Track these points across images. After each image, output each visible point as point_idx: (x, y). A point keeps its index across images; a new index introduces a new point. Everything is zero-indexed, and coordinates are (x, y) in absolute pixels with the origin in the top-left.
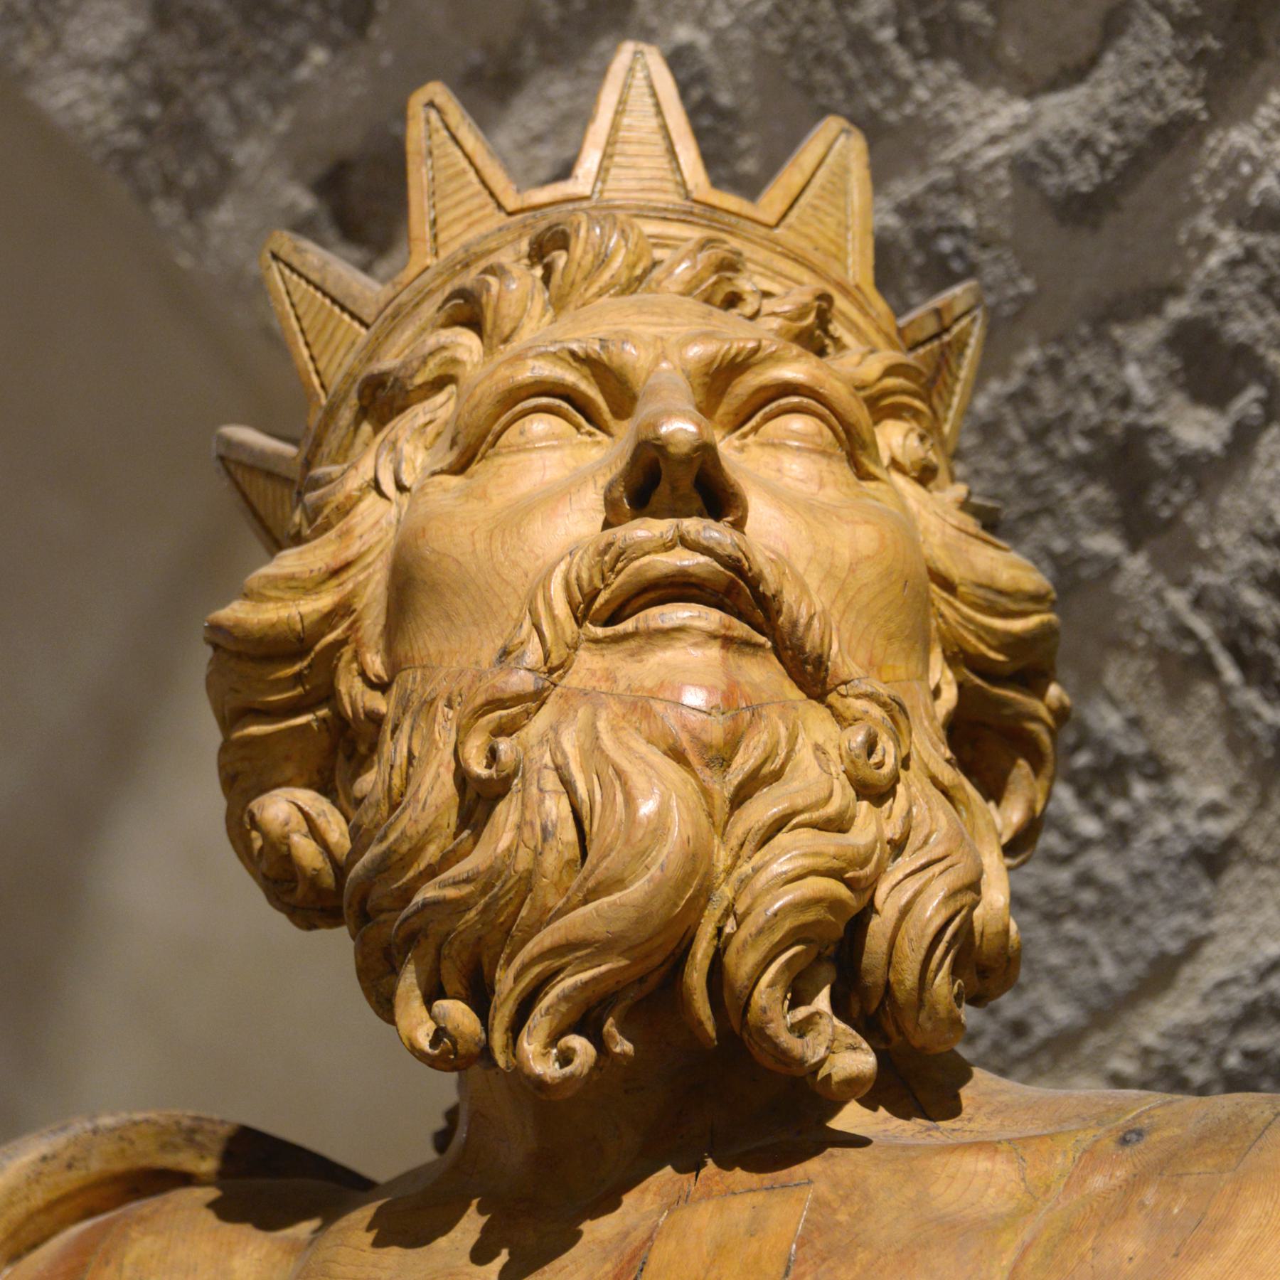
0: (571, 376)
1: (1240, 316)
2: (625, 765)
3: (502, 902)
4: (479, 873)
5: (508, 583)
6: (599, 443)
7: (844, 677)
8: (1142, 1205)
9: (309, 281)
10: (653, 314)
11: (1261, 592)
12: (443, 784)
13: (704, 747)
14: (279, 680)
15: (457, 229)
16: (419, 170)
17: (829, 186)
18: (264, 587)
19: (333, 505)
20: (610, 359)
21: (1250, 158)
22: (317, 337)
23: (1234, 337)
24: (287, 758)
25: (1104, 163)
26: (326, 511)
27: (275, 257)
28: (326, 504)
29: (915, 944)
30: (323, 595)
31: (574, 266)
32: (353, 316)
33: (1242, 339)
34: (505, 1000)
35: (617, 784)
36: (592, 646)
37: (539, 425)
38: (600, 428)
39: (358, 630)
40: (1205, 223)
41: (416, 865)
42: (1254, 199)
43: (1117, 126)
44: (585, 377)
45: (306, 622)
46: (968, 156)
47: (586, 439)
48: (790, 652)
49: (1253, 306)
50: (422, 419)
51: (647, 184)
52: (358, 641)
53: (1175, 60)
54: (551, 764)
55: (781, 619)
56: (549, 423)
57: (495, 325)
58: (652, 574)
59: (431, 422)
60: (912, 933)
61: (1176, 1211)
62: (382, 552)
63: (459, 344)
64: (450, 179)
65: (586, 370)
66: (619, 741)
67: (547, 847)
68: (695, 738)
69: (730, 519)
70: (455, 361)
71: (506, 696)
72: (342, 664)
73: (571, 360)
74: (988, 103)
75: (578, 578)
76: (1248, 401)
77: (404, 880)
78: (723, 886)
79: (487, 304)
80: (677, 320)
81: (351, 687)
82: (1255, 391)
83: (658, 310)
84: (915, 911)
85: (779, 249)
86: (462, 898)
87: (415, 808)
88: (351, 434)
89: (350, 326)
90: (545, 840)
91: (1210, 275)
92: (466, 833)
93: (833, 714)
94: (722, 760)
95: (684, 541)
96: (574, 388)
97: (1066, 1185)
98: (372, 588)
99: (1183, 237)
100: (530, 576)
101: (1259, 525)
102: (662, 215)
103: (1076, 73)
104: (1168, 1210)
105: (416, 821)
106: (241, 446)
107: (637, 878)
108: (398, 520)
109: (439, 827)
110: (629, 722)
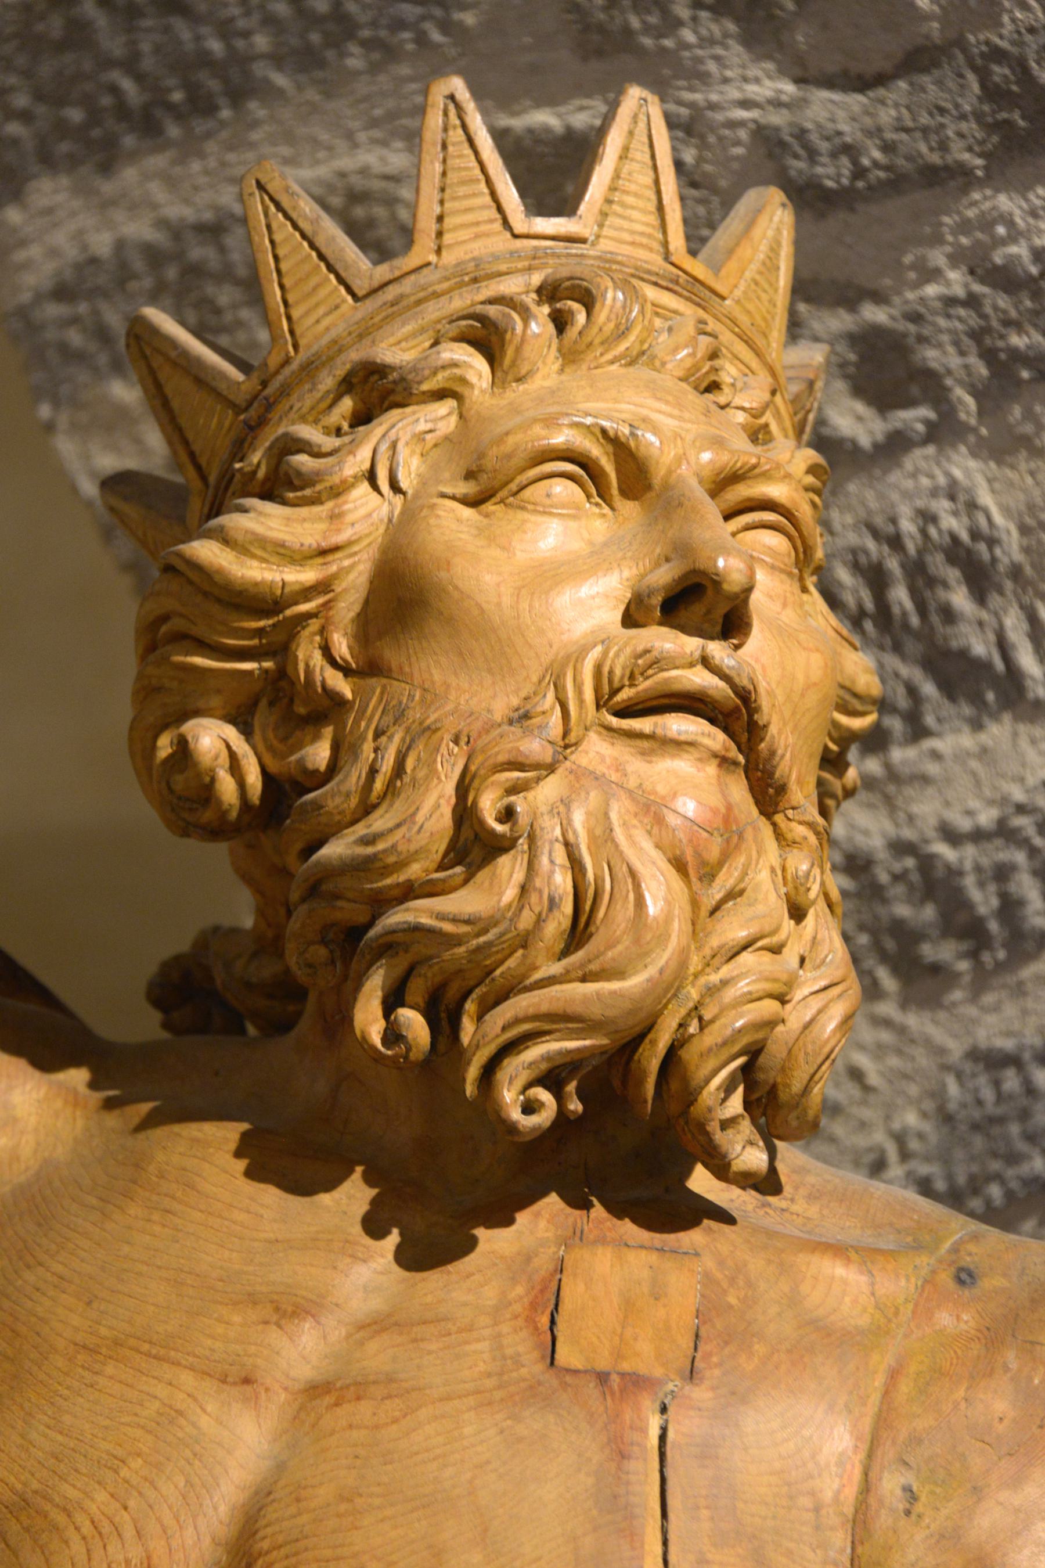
0: (596, 451)
1: (940, 346)
2: (638, 866)
3: (494, 949)
4: (480, 919)
5: (530, 646)
6: (604, 515)
7: (794, 803)
8: (1006, 1369)
9: (295, 226)
10: (667, 402)
11: (854, 575)
12: (442, 815)
13: (704, 863)
14: (243, 629)
15: (463, 235)
16: (432, 162)
17: (768, 262)
18: (251, 543)
19: (328, 484)
20: (637, 447)
21: (1010, 223)
22: (296, 284)
23: (924, 359)
24: (219, 691)
25: (859, 172)
26: (319, 487)
27: (260, 186)
28: (320, 481)
29: (810, 1059)
30: (307, 568)
31: (595, 330)
32: (341, 280)
33: (933, 365)
34: (489, 1042)
35: (629, 881)
36: (604, 732)
37: (561, 488)
38: (605, 501)
39: (330, 608)
40: (938, 258)
41: (395, 876)
42: (998, 258)
43: (888, 148)
44: (607, 454)
45: (287, 590)
46: (713, 107)
47: (596, 510)
48: (759, 774)
49: (956, 343)
50: (422, 426)
51: (638, 239)
52: (327, 619)
53: (971, 118)
54: (561, 838)
55: (763, 745)
56: (566, 487)
57: (514, 363)
58: (677, 687)
59: (430, 431)
60: (810, 1048)
61: (1036, 1381)
62: (369, 544)
63: (471, 367)
64: (463, 183)
65: (610, 448)
66: (630, 837)
67: (551, 917)
68: (698, 854)
69: (735, 641)
70: (463, 381)
71: (528, 762)
72: (306, 633)
73: (600, 436)
74: (753, 72)
75: (611, 672)
76: (915, 417)
77: (380, 884)
78: (689, 987)
79: (511, 341)
80: (687, 415)
81: (310, 657)
82: (925, 412)
83: (670, 398)
84: (815, 1028)
85: (737, 330)
86: (458, 935)
87: (409, 829)
88: (329, 401)
89: (336, 289)
90: (550, 909)
91: (922, 300)
92: (458, 869)
93: (775, 831)
94: (709, 875)
95: (705, 661)
96: (596, 462)
97: (914, 1312)
98: (355, 576)
99: (908, 259)
100: (555, 647)
101: (879, 521)
102: (654, 279)
103: (861, 84)
104: (1030, 1379)
105: (409, 840)
106: (154, 331)
107: (636, 972)
108: (390, 520)
109: (429, 851)
110: (641, 822)
